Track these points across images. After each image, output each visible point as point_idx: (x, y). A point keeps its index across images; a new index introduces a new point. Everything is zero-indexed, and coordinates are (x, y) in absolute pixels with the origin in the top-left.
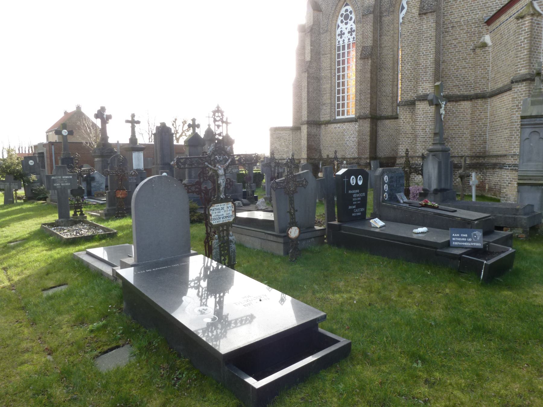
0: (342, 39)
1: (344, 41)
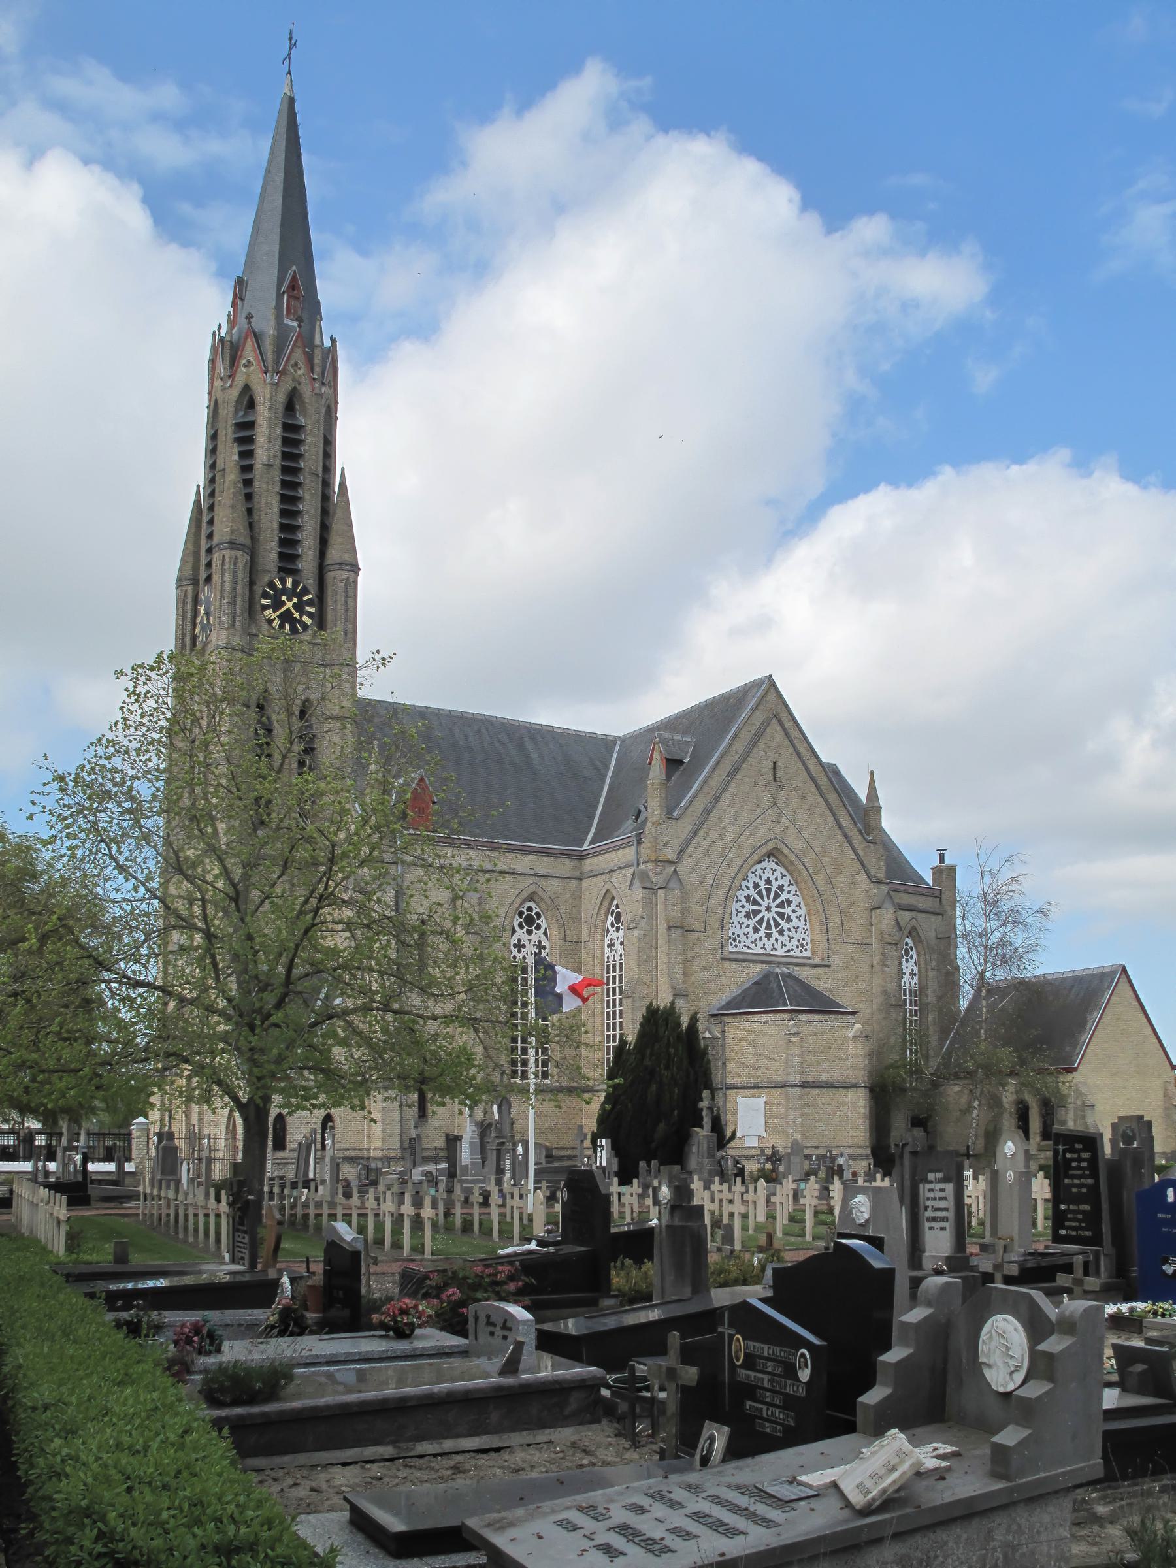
0: (521, 955)
1: (524, 958)
